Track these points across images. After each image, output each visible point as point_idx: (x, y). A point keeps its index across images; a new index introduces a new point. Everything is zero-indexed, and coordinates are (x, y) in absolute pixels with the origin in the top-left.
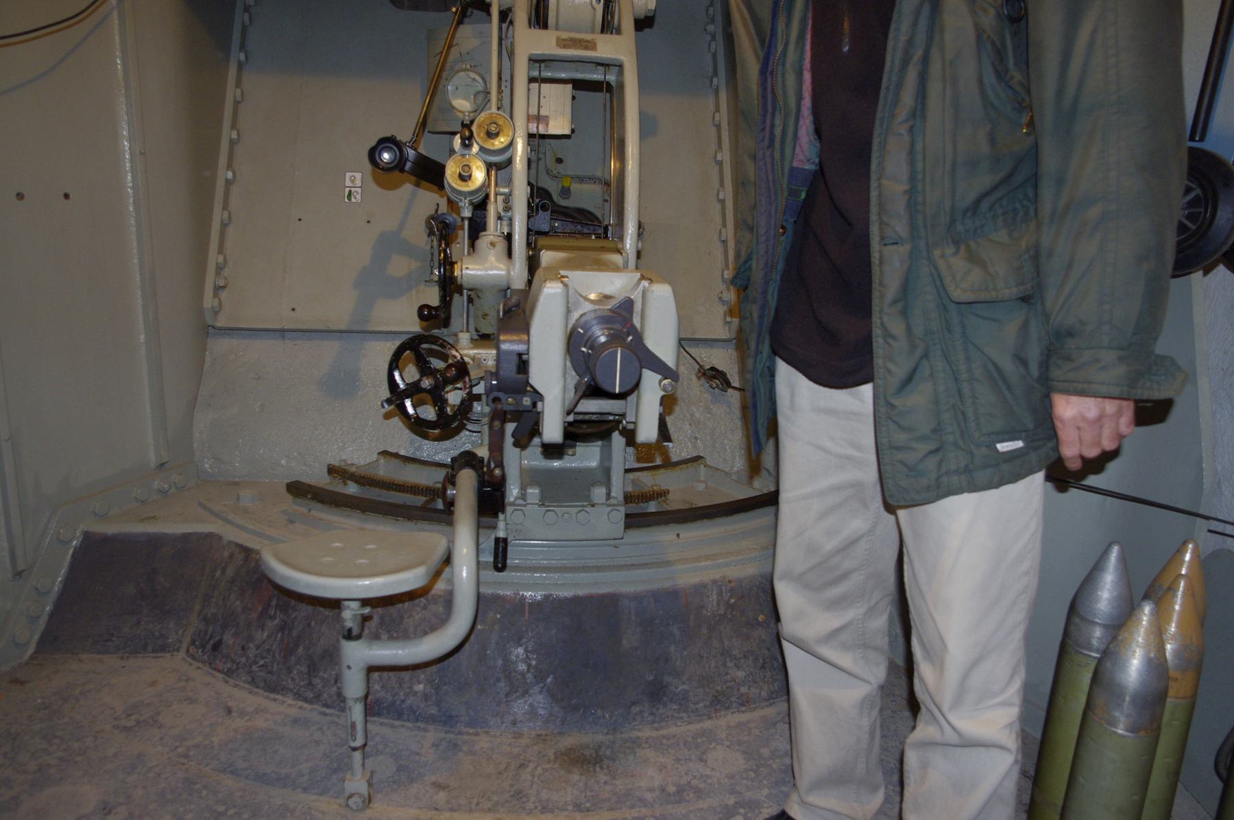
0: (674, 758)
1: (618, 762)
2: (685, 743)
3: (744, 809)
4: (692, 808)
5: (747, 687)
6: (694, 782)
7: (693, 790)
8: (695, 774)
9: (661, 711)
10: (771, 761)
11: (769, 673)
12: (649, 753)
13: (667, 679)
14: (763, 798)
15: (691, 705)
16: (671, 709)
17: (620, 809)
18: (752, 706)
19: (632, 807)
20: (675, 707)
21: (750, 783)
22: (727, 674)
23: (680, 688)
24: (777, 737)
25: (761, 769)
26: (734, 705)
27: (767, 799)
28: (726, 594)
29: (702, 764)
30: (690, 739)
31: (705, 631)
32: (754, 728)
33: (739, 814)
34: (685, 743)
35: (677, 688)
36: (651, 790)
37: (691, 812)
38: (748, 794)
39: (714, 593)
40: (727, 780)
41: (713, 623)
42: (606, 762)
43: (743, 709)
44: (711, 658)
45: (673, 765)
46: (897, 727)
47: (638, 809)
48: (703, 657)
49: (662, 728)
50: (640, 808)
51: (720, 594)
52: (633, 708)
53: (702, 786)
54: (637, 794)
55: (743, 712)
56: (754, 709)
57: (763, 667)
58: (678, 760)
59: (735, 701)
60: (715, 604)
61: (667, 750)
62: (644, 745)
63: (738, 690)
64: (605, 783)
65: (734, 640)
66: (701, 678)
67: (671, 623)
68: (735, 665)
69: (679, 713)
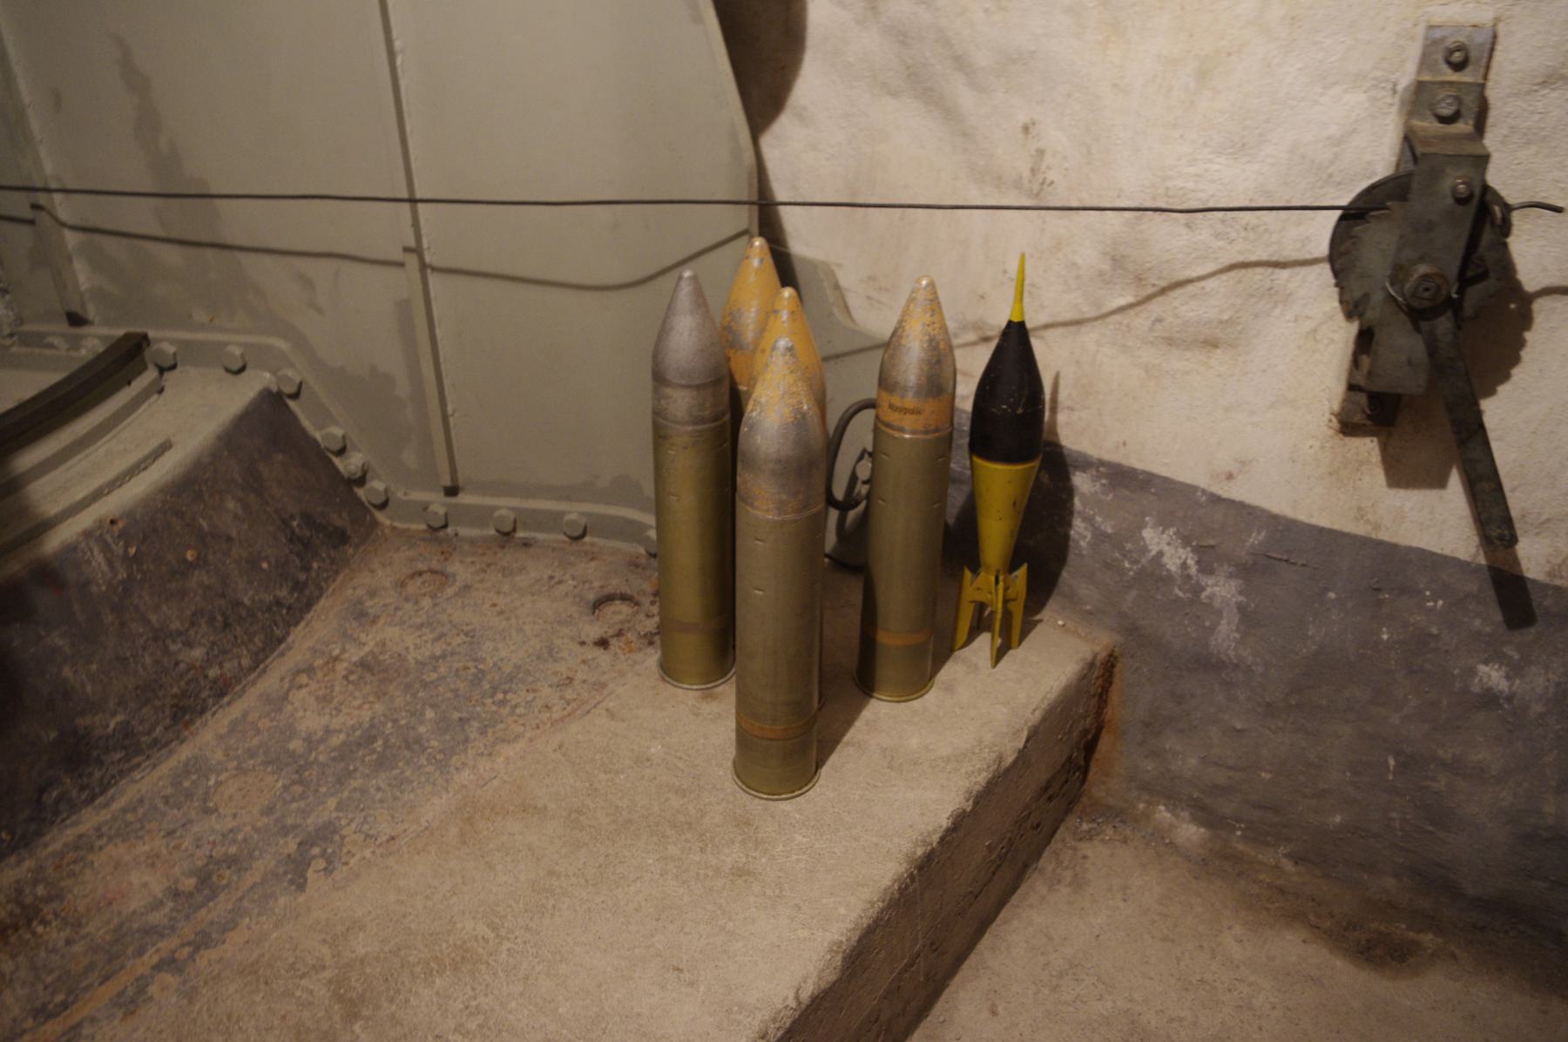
0: (162, 833)
1: (70, 896)
2: (166, 800)
3: (317, 845)
4: (239, 894)
5: (217, 667)
6: (218, 852)
7: (224, 865)
8: (211, 839)
9: (97, 775)
10: (314, 754)
11: (238, 629)
12: (118, 850)
13: (82, 722)
14: (334, 815)
15: (144, 739)
16: (113, 763)
17: (122, 968)
18: (238, 688)
19: (140, 952)
20: (118, 756)
21: (302, 804)
22: (177, 664)
23: (112, 725)
24: (301, 714)
25: (307, 773)
26: (210, 701)
27: (341, 811)
28: (117, 545)
29: (214, 817)
30: (169, 791)
31: (109, 618)
32: (260, 718)
33: (315, 857)
34: (166, 800)
35: (107, 726)
36: (157, 905)
37: (241, 899)
38: (309, 821)
39: (96, 552)
40: (265, 820)
41: (116, 599)
42: (47, 910)
43: (226, 699)
44: (140, 653)
45: (168, 845)
46: (450, 615)
47: (154, 949)
48: (126, 659)
49: (113, 799)
50: (154, 945)
51: (106, 548)
52: (45, 797)
53: (233, 850)
54: (135, 926)
55: (229, 704)
56: (243, 691)
57: (226, 625)
58: (170, 833)
59: (209, 696)
60: (105, 567)
61: (142, 827)
62: (99, 843)
63: (206, 677)
64: (69, 942)
65: (164, 608)
66: (139, 692)
67: (43, 633)
68: (184, 644)
69: (129, 760)
